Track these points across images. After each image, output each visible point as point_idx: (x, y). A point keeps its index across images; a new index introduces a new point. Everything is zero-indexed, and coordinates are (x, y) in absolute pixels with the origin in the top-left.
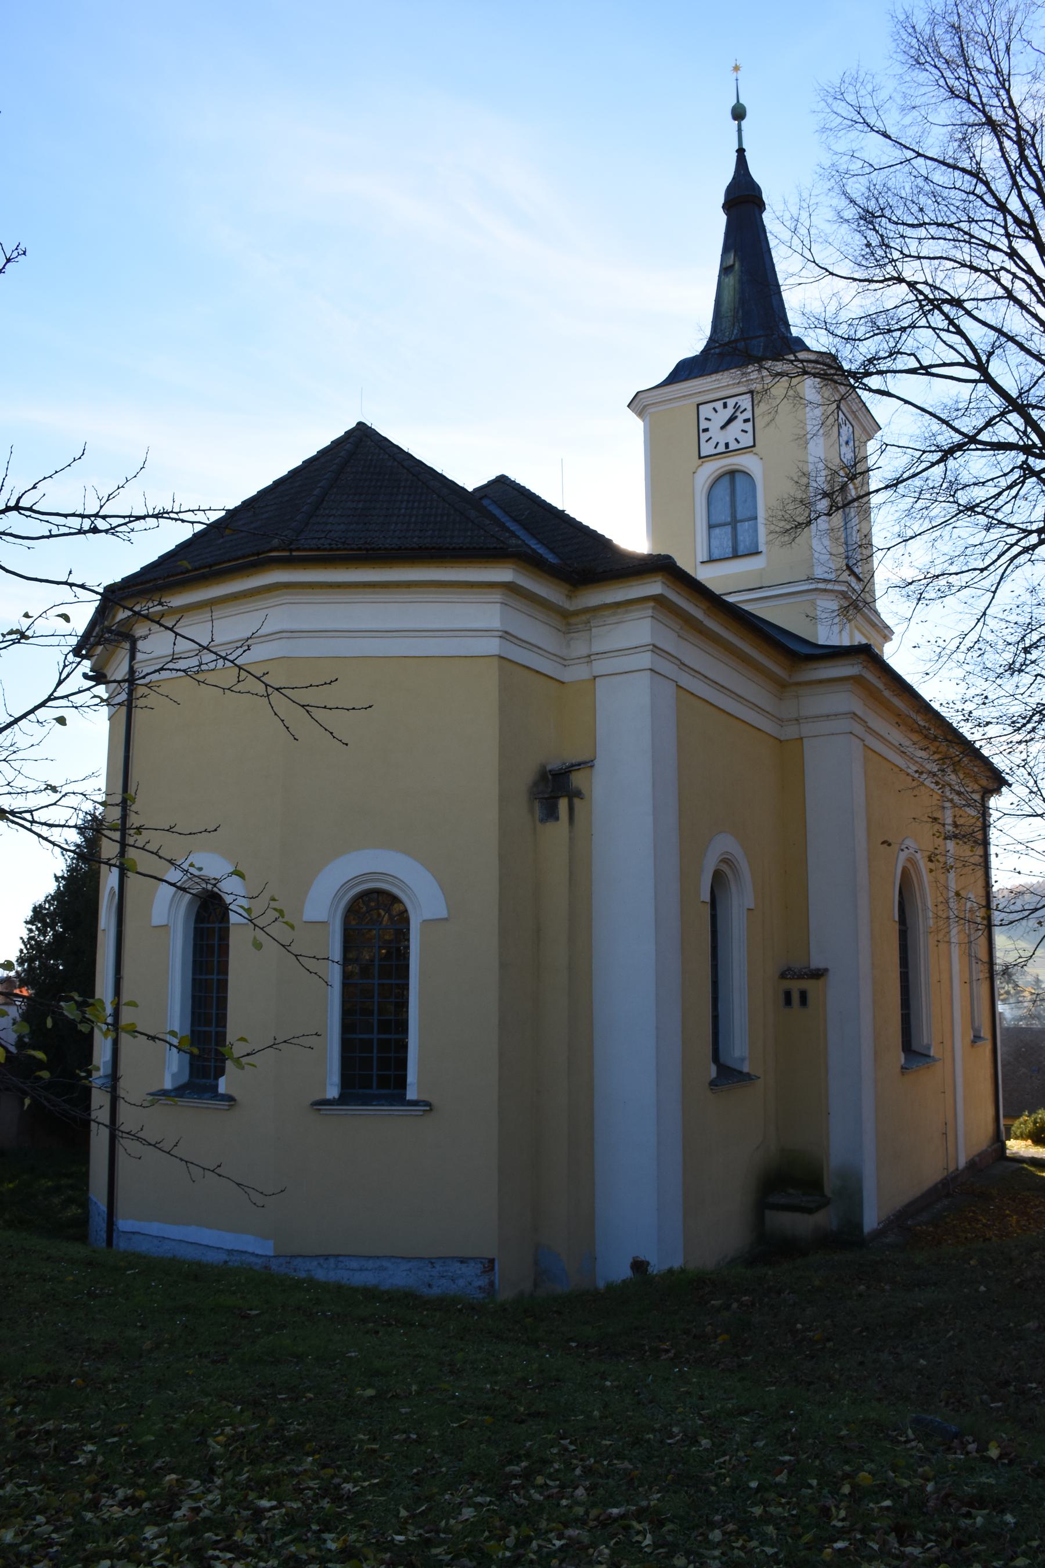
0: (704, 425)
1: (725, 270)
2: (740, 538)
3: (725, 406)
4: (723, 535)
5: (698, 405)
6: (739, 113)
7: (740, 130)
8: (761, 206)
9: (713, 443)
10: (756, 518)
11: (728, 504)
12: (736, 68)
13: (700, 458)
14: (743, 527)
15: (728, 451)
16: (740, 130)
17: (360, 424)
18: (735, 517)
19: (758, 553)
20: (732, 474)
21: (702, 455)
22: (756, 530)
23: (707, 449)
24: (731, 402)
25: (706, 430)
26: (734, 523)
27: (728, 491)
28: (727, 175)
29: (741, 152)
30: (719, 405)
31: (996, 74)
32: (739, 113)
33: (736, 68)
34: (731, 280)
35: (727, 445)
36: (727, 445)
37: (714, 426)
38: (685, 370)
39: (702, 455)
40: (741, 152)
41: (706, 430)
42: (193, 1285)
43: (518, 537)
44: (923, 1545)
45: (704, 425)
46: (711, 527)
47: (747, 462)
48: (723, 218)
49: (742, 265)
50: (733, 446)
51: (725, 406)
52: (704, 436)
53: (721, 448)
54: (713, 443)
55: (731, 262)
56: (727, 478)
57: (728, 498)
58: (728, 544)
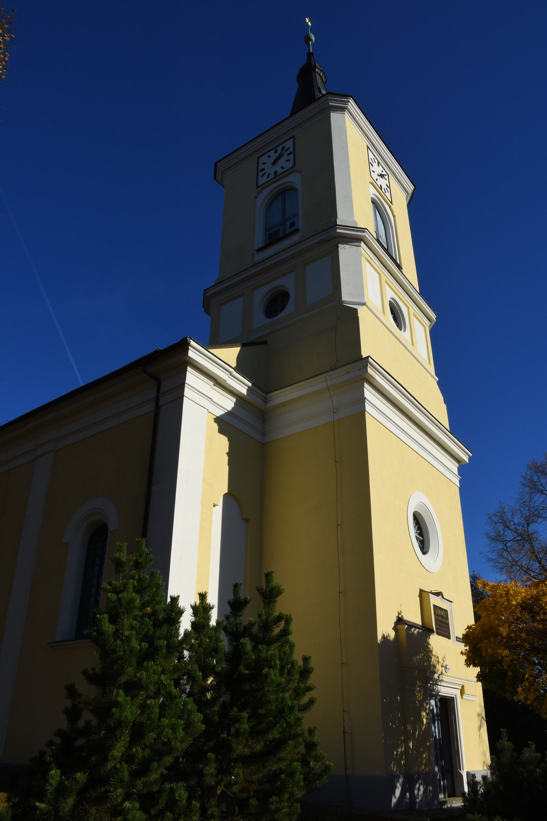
23: (262, 180)
47: (295, 179)
54: (266, 175)
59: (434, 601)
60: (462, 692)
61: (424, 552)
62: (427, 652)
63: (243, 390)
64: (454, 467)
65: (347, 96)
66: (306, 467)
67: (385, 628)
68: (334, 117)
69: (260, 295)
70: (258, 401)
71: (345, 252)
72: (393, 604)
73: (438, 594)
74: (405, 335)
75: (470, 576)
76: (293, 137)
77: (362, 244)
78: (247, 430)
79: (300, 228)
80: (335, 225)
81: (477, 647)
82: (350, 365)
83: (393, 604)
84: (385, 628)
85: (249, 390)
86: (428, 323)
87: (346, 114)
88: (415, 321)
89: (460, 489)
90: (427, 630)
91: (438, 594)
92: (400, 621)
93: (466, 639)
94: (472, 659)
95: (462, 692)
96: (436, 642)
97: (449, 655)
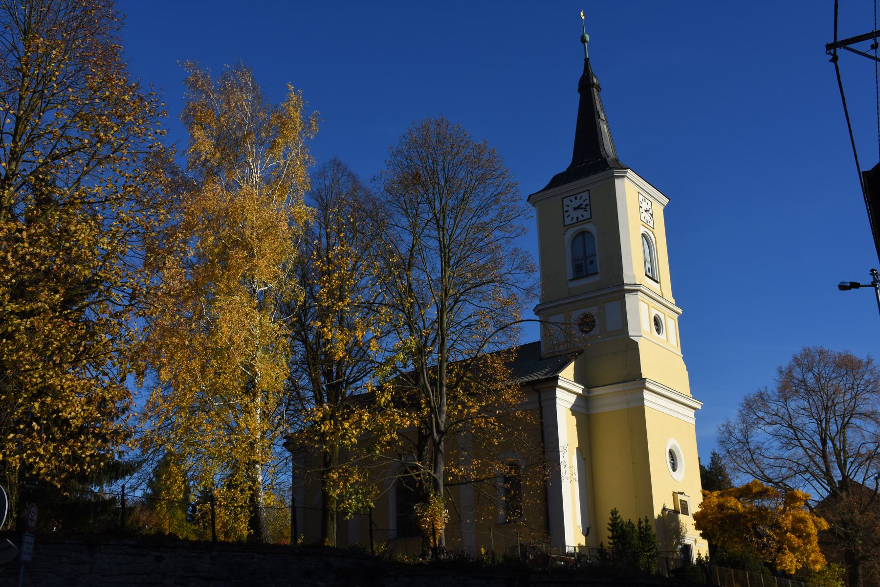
0: (566, 208)
9: (570, 218)
17: (571, 409)
20: (583, 233)
23: (568, 221)
25: (567, 211)
30: (573, 198)
35: (577, 219)
36: (577, 219)
38: (558, 181)
41: (567, 211)
43: (813, 521)
44: (489, 439)
45: (566, 208)
47: (590, 227)
48: (579, 95)
50: (581, 219)
52: (566, 214)
53: (575, 220)
54: (570, 218)
59: (680, 497)
60: (695, 542)
61: (674, 470)
62: (678, 522)
63: (580, 392)
64: (691, 413)
65: (626, 169)
66: (616, 431)
67: (657, 512)
68: (617, 182)
69: (576, 315)
70: (586, 394)
71: (629, 299)
72: (661, 501)
73: (682, 493)
74: (663, 336)
75: (702, 468)
77: (639, 293)
78: (583, 410)
79: (599, 271)
80: (623, 284)
81: (701, 521)
82: (634, 379)
83: (661, 501)
84: (657, 512)
85: (583, 390)
86: (677, 316)
87: (626, 179)
88: (669, 319)
89: (696, 426)
90: (676, 512)
91: (682, 493)
92: (664, 509)
93: (695, 517)
94: (698, 527)
95: (695, 542)
96: (681, 517)
97: (687, 522)
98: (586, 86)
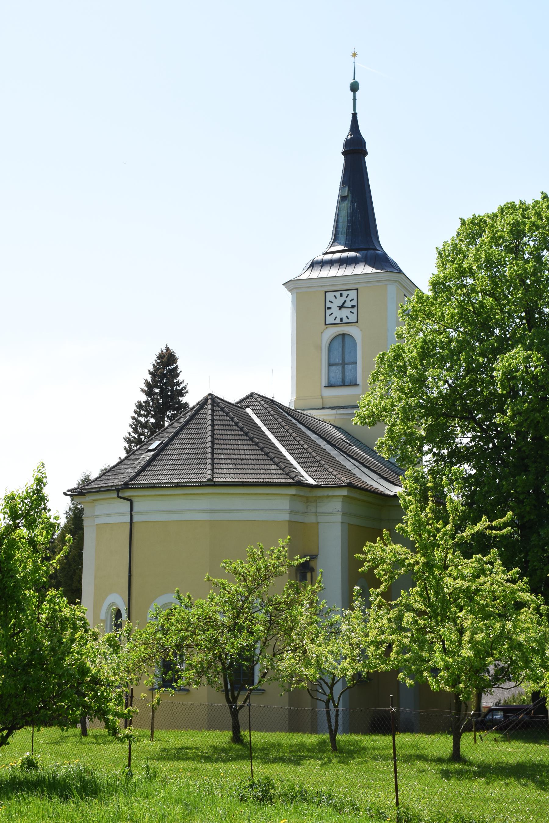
0: (328, 305)
1: (342, 199)
2: (347, 374)
3: (341, 295)
4: (337, 371)
5: (326, 292)
6: (354, 87)
7: (354, 99)
8: (366, 153)
9: (333, 317)
10: (356, 363)
11: (340, 353)
12: (355, 55)
13: (326, 324)
14: (348, 367)
15: (342, 323)
16: (354, 99)
18: (344, 361)
19: (356, 385)
20: (344, 335)
21: (327, 323)
22: (356, 370)
23: (330, 320)
24: (345, 293)
26: (344, 364)
27: (341, 345)
28: (344, 132)
29: (355, 115)
31: (327, 703)
32: (354, 87)
33: (355, 55)
34: (345, 204)
35: (341, 319)
36: (341, 319)
37: (335, 310)
39: (327, 323)
40: (355, 115)
41: (329, 308)
42: (449, 733)
46: (330, 365)
49: (352, 197)
50: (345, 320)
51: (341, 295)
53: (338, 321)
54: (333, 317)
55: (346, 194)
56: (340, 337)
57: (340, 349)
58: (339, 376)
76: (357, 289)
79: (359, 381)
98: (355, 150)
